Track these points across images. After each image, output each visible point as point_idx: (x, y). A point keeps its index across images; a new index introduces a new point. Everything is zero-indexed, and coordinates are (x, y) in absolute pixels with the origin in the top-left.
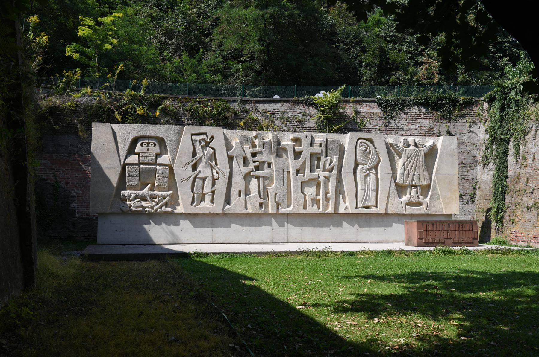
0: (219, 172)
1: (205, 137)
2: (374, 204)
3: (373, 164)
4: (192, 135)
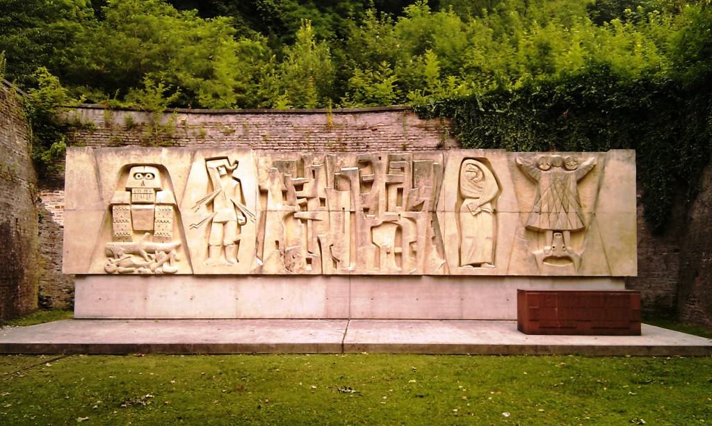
0: (245, 213)
1: (224, 162)
2: (489, 259)
3: (491, 197)
4: (207, 160)
